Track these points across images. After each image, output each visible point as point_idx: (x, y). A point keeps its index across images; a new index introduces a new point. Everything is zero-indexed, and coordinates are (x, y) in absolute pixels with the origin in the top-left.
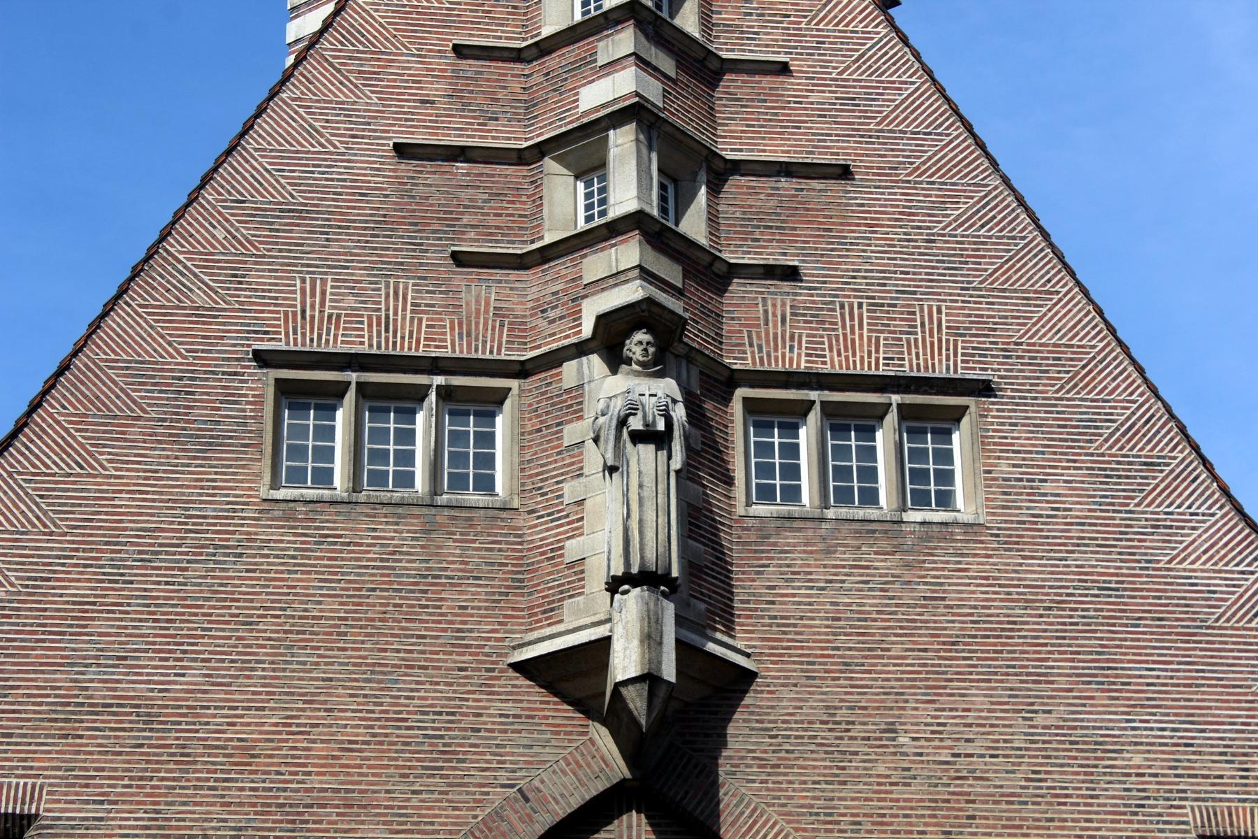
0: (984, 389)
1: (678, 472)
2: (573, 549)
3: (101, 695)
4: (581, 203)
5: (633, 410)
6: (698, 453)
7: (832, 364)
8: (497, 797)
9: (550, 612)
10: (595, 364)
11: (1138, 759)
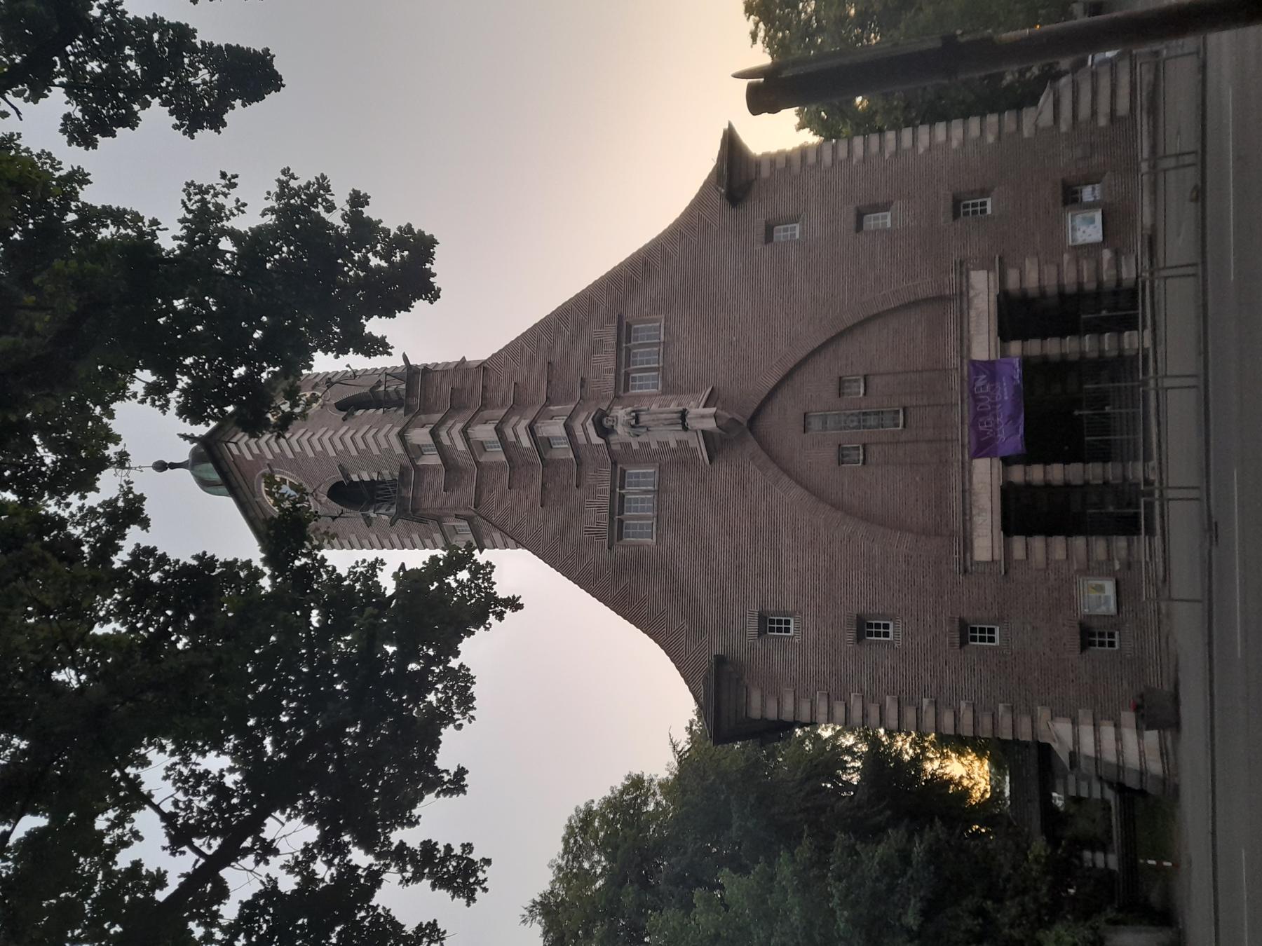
0: (620, 317)
1: (1136, 459)
2: (673, 444)
7: (612, 366)
9: (694, 451)
10: (613, 438)
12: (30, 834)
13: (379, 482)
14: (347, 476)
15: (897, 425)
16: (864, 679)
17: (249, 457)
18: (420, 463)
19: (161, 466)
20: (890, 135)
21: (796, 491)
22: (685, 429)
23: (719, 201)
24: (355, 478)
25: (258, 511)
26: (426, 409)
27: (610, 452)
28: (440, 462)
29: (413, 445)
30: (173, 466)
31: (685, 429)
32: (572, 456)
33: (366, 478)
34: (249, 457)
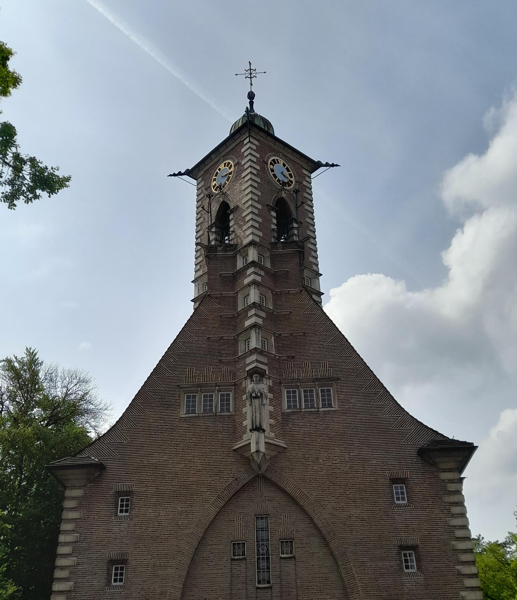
0: (338, 379)
3: (146, 463)
4: (266, 345)
5: (253, 391)
6: (272, 399)
8: (231, 480)
9: (241, 438)
11: (375, 462)
14: (232, 211)
15: (259, 582)
16: (86, 566)
17: (243, 150)
18: (238, 256)
19: (251, 96)
21: (213, 511)
23: (423, 442)
24: (231, 217)
25: (216, 160)
26: (273, 258)
29: (247, 250)
30: (251, 103)
34: (243, 150)
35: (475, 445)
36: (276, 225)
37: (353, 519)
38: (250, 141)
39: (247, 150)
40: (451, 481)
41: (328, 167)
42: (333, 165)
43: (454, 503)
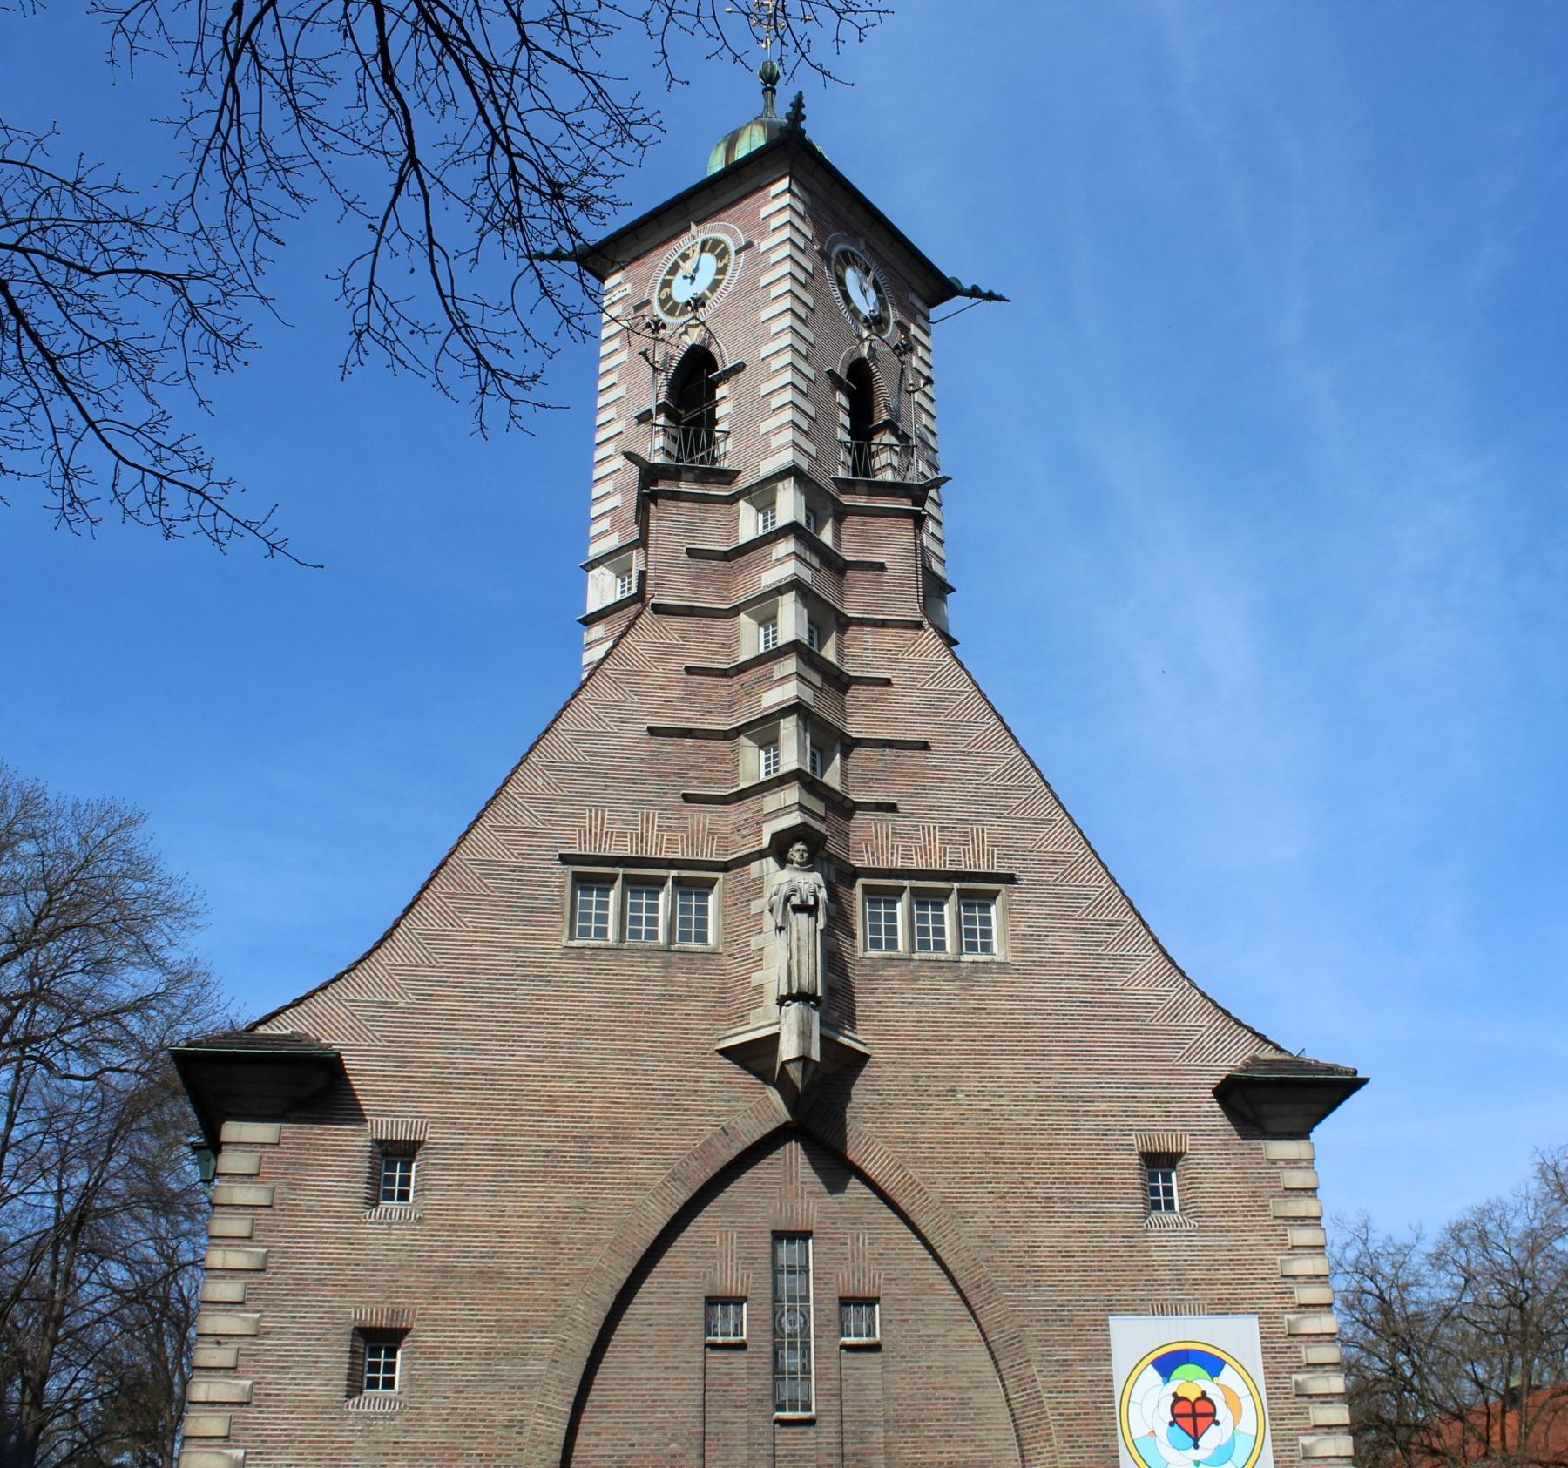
0: (1010, 879)
2: (756, 978)
7: (916, 864)
9: (742, 1017)
10: (770, 863)
11: (1103, 1106)
12: (774, 835)
13: (710, 435)
20: (1337, 1384)
22: (781, 1001)
24: (721, 391)
27: (744, 861)
28: (742, 541)
29: (774, 491)
31: (781, 1001)
32: (742, 786)
33: (720, 412)
34: (764, 212)
35: (1359, 1076)
36: (850, 433)
37: (1044, 1251)
38: (789, 190)
39: (780, 210)
40: (1293, 1163)
41: (975, 300)
42: (990, 296)
43: (1295, 1219)
